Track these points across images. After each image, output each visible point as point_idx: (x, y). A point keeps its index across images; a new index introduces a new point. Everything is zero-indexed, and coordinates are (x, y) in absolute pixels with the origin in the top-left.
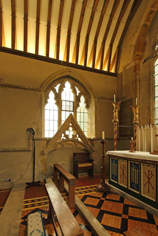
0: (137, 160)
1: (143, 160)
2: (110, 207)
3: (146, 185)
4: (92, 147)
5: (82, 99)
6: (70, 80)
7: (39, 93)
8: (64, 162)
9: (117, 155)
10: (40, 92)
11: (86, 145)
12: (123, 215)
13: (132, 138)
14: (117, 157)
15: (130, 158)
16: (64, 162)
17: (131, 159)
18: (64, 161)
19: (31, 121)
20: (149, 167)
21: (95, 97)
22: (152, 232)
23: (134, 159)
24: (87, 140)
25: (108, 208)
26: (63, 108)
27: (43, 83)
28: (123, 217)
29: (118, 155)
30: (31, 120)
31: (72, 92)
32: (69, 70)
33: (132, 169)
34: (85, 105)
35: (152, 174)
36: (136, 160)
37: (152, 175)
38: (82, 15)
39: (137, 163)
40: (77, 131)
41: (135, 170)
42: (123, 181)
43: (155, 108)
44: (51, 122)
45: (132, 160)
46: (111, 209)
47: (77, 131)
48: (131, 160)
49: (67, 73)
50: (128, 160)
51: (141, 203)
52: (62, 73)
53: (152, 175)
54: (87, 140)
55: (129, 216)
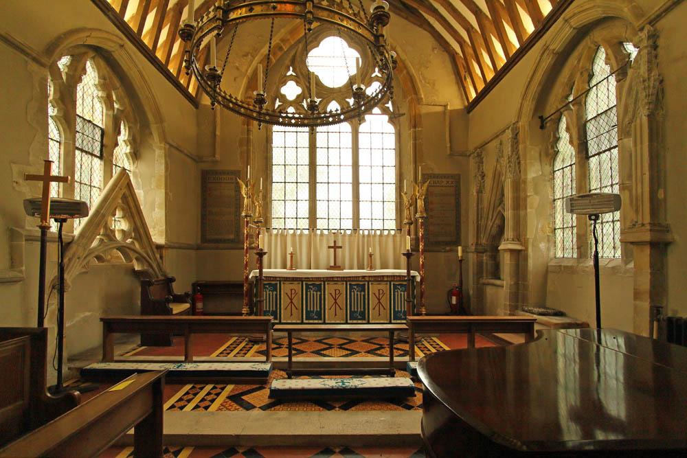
4: (160, 261)
5: (124, 136)
6: (102, 63)
7: (34, 67)
8: (87, 314)
10: (42, 68)
11: (150, 261)
13: (460, 248)
15: (306, 278)
16: (87, 314)
17: (307, 279)
18: (89, 311)
19: (13, 166)
21: (164, 138)
24: (154, 247)
26: (592, 149)
30: (14, 163)
32: (122, 43)
34: (128, 149)
36: (318, 279)
38: (636, 163)
40: (135, 223)
47: (135, 223)
49: (113, 45)
50: (302, 282)
52: (106, 39)
54: (154, 247)
55: (200, 407)
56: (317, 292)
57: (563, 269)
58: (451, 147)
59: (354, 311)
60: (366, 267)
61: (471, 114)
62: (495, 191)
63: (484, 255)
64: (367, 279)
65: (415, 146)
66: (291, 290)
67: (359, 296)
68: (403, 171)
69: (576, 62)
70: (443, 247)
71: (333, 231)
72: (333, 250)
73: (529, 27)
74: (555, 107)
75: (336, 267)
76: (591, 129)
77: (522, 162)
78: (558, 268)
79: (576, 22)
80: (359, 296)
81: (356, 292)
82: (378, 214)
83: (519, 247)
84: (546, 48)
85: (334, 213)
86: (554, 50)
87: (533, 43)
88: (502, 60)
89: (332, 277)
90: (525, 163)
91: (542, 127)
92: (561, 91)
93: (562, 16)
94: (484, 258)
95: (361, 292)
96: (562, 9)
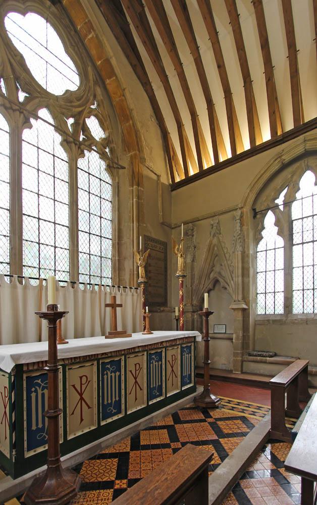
0: (89, 357)
1: (71, 358)
2: (146, 459)
3: (132, 392)
9: (64, 354)
12: (171, 444)
14: (123, 353)
20: (83, 368)
22: (149, 462)
23: (114, 351)
25: (160, 455)
26: (297, 239)
27: (247, 198)
28: (178, 443)
29: (68, 354)
31: (61, 144)
33: (33, 395)
35: (88, 380)
36: (118, 353)
37: (88, 382)
38: (221, 67)
39: (39, 374)
41: (157, 363)
42: (82, 420)
43: (258, 273)
44: (270, 289)
45: (109, 355)
46: (154, 455)
48: (106, 356)
50: (98, 361)
51: (130, 428)
53: (88, 382)
55: (206, 421)
56: (158, 362)
57: (271, 322)
58: (163, 215)
59: (108, 403)
60: (129, 332)
61: (174, 192)
62: (208, 261)
63: (195, 314)
64: (165, 345)
65: (138, 204)
66: (81, 378)
67: (157, 365)
68: (122, 227)
69: (290, 176)
70: (158, 307)
71: (62, 284)
72: (118, 302)
73: (266, 135)
74: (266, 205)
75: (114, 334)
76: (297, 226)
77: (246, 240)
78: (266, 321)
79: (309, 146)
80: (157, 365)
81: (109, 374)
82: (95, 270)
83: (245, 306)
84: (279, 156)
85: (47, 263)
86: (284, 160)
87: (266, 149)
88: (226, 154)
89: (134, 348)
90: (248, 241)
91: (255, 217)
92: (273, 194)
93: (304, 135)
94: (195, 316)
95: (115, 372)
96: (305, 131)
